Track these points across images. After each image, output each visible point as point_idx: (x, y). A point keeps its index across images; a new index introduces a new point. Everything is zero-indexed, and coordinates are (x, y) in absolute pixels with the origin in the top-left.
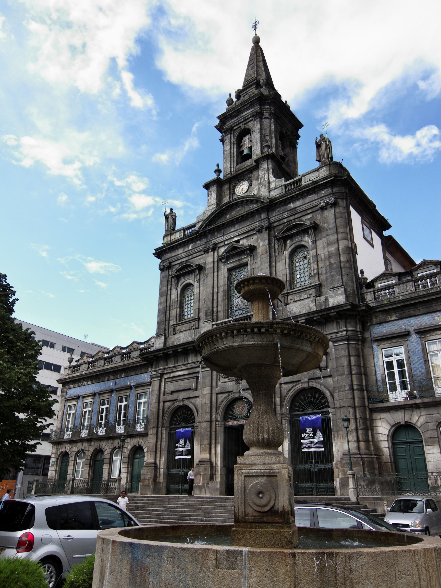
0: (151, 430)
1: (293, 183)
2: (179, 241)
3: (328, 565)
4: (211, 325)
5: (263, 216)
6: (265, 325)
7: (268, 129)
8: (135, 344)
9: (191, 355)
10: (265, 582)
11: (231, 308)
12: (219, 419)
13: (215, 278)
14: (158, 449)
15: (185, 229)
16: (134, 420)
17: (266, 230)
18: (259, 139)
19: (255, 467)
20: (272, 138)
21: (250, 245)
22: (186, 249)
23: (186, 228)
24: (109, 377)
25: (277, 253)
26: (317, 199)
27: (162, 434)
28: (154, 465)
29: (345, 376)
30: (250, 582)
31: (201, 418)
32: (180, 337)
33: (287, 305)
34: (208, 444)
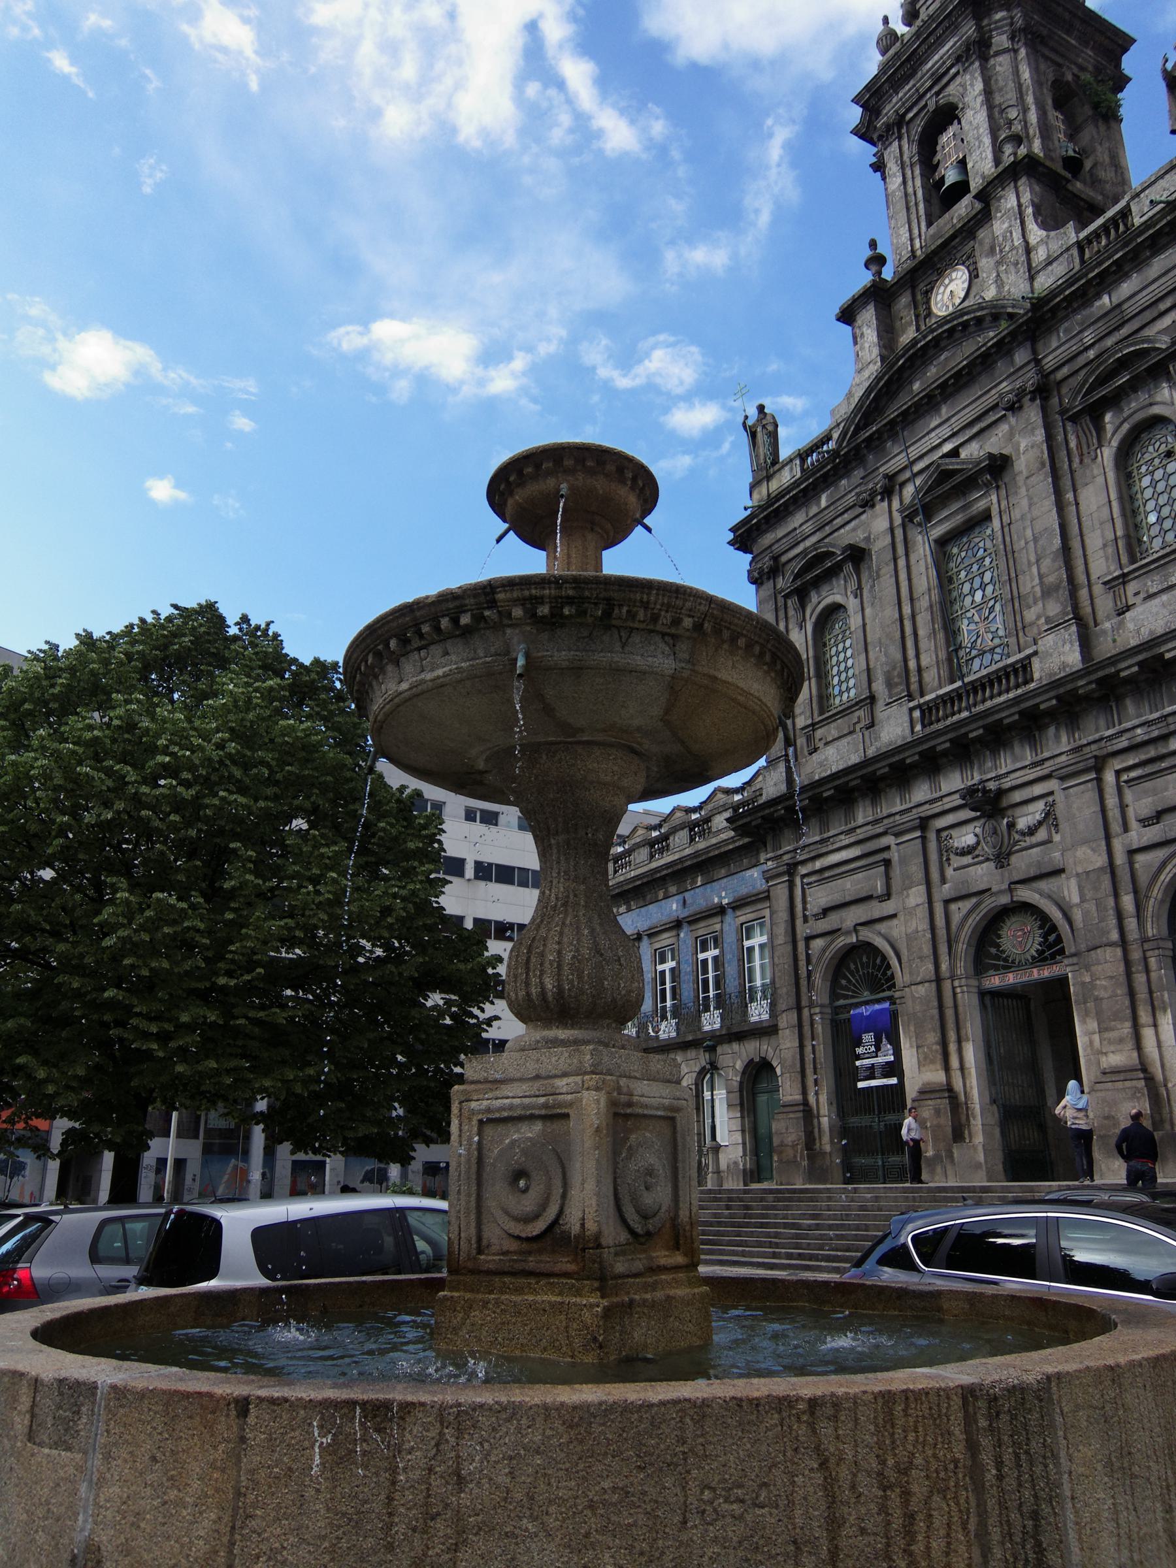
0: (784, 1015)
1: (1105, 228)
2: (789, 492)
3: (364, 1453)
4: (905, 709)
5: (1021, 356)
6: (470, 601)
7: (1011, 85)
8: (720, 795)
9: (861, 804)
10: (142, 1502)
11: (956, 651)
12: (960, 971)
13: (903, 576)
14: (807, 1066)
15: (803, 455)
16: (742, 992)
17: (1033, 400)
18: (986, 125)
19: (507, 1090)
20: (1025, 110)
21: (991, 456)
22: (814, 510)
23: (806, 451)
24: (666, 889)
25: (1076, 460)
27: (812, 1025)
28: (801, 1108)
30: (102, 1499)
31: (910, 973)
32: (826, 759)
33: (1123, 613)
34: (937, 1043)
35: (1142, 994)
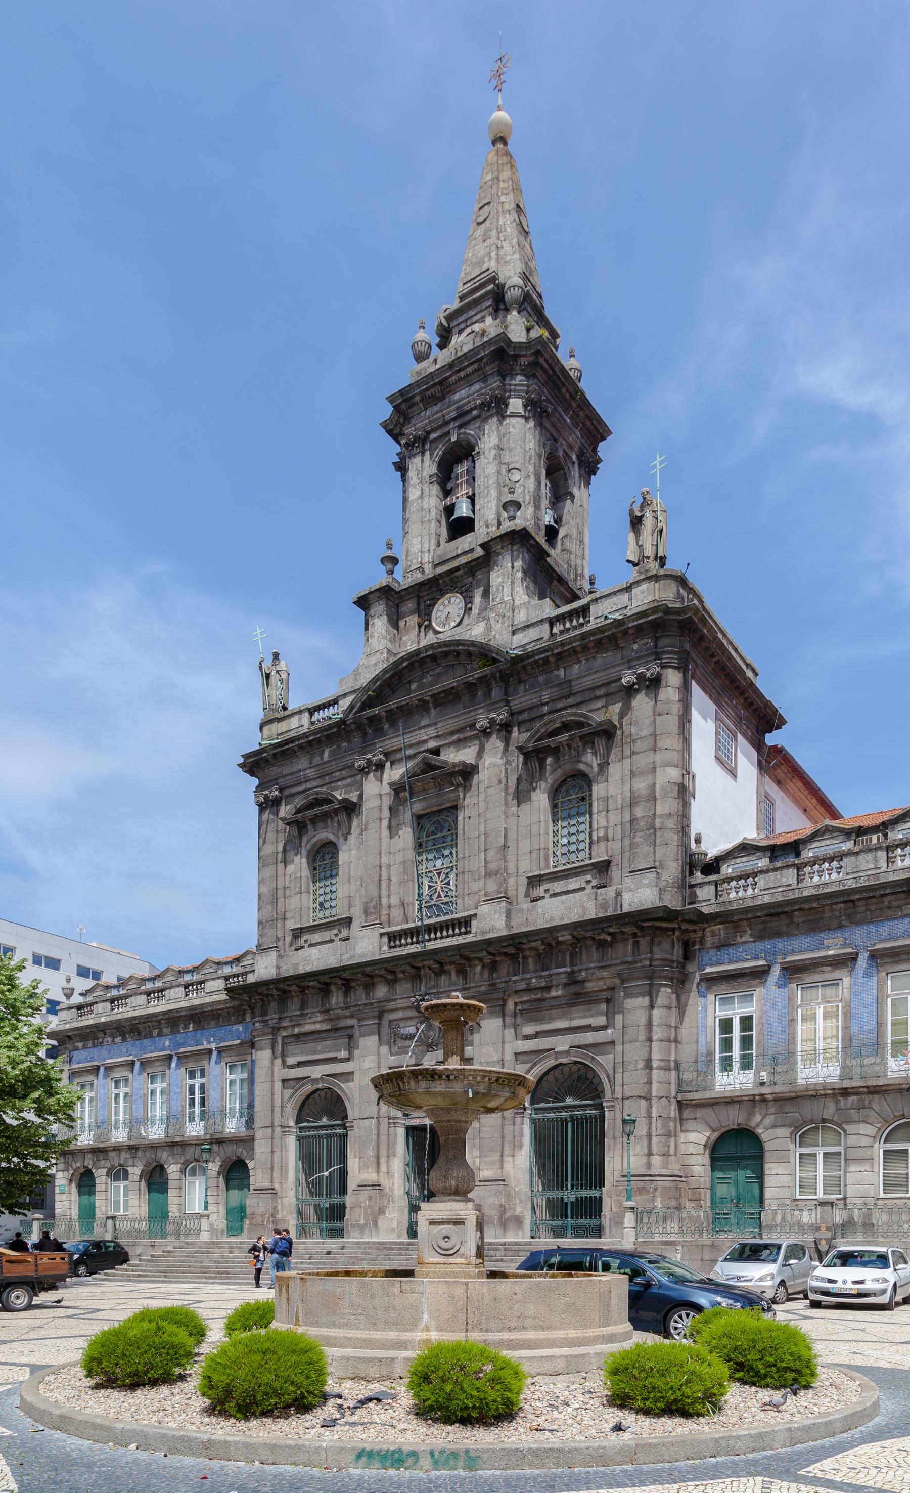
23: (315, 707)
26: (618, 665)
29: (638, 1044)
32: (310, 956)
35: (508, 1138)
